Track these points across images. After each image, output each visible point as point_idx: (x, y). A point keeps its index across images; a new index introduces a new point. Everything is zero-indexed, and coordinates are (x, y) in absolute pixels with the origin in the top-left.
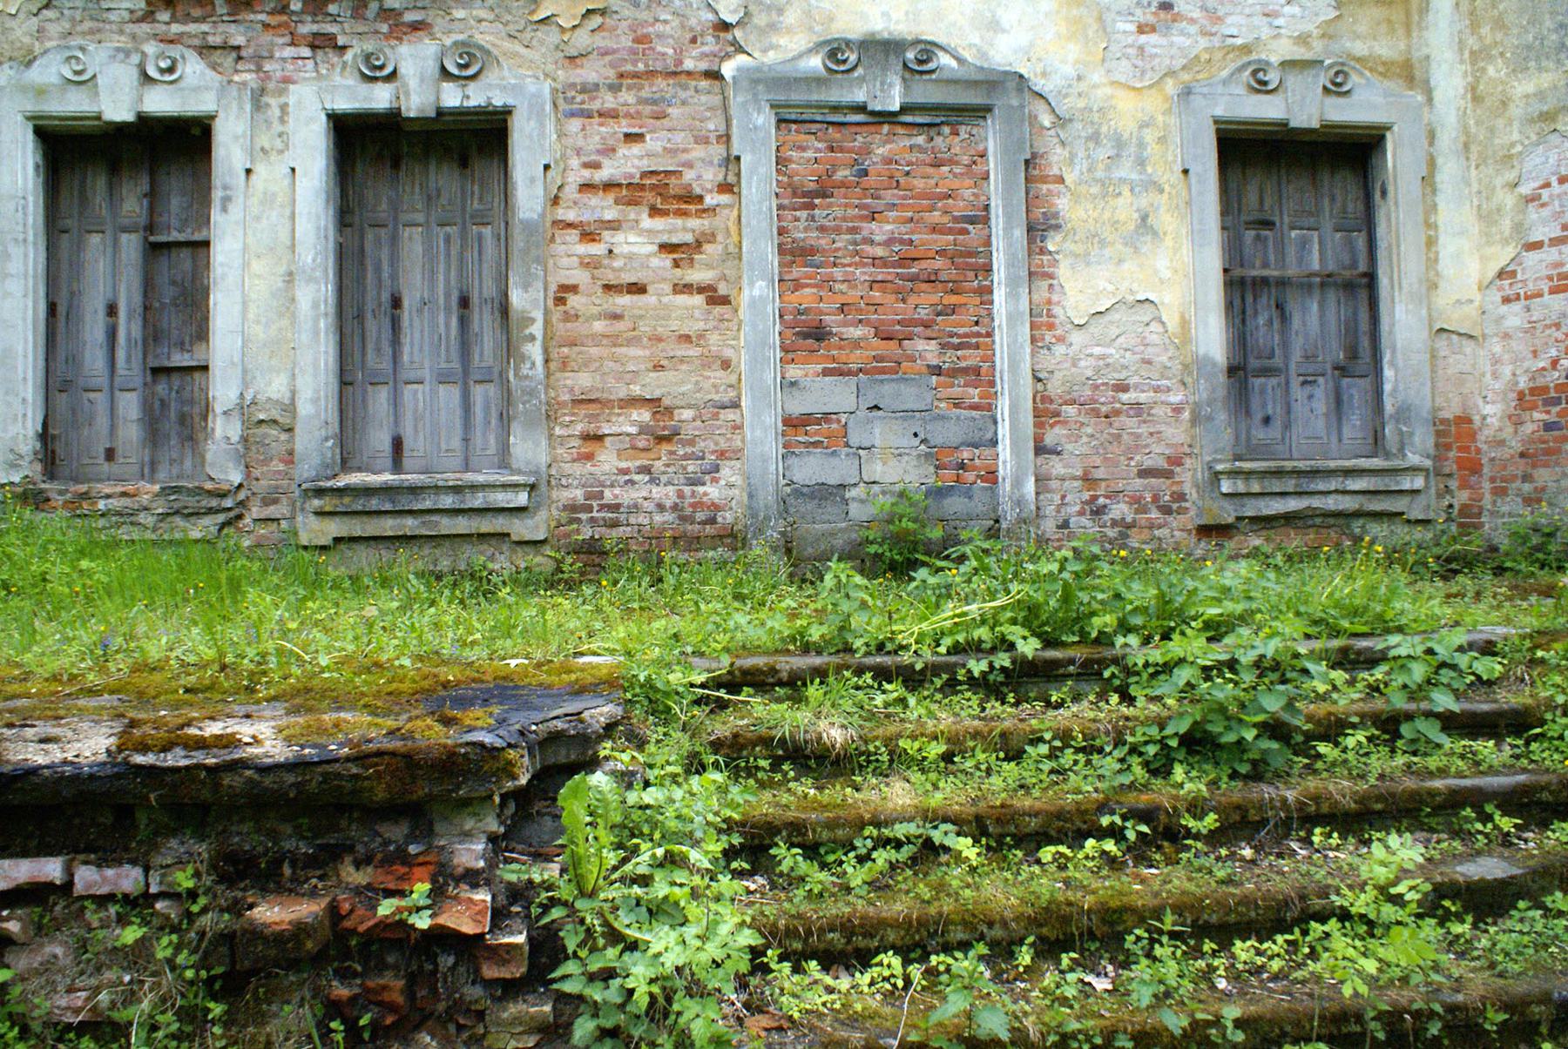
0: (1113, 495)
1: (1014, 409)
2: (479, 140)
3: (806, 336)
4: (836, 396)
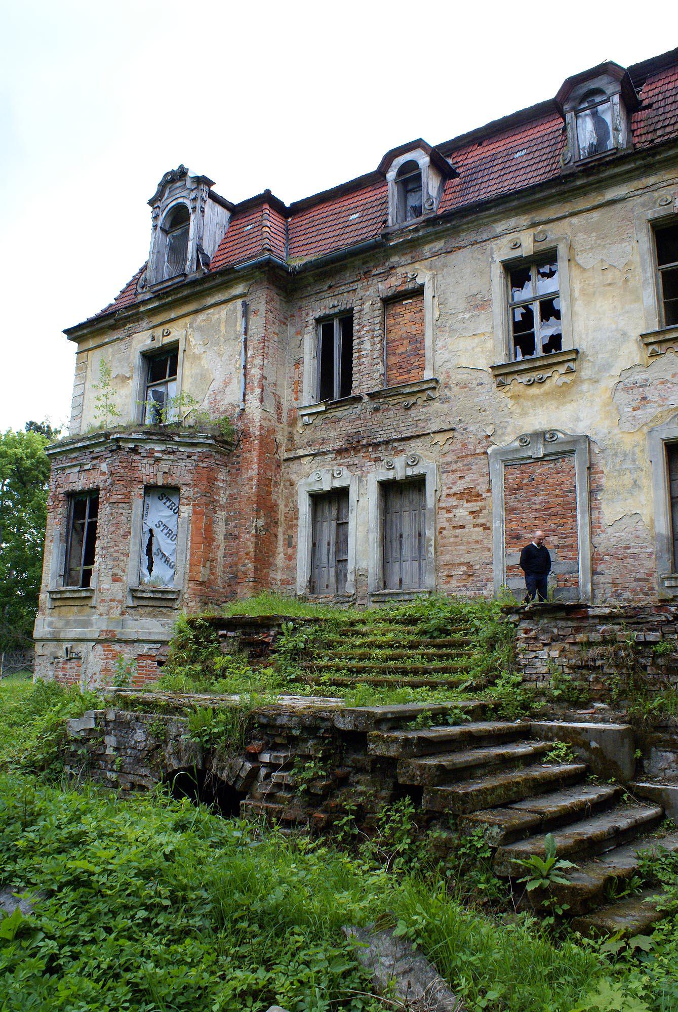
0: (625, 589)
1: (583, 558)
2: (417, 484)
3: (513, 538)
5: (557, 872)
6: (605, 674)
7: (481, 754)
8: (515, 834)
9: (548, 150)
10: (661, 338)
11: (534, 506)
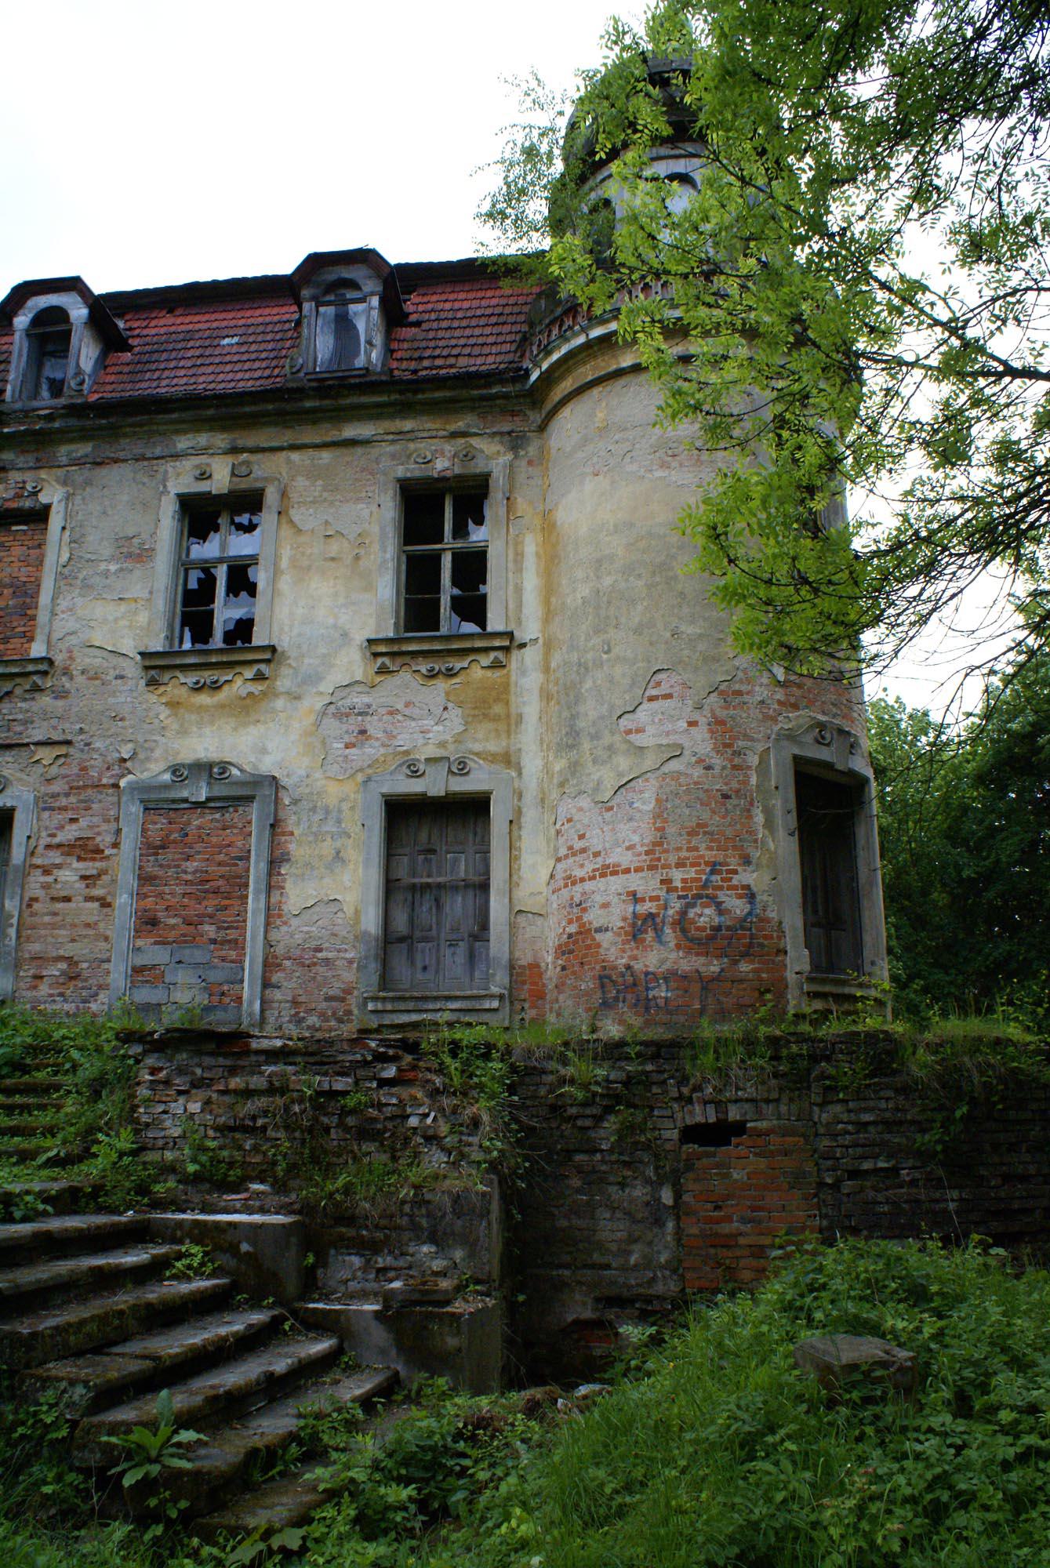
0: (309, 1011)
3: (147, 923)
4: (158, 955)
5: (174, 1450)
6: (268, 1140)
7: (64, 1267)
8: (110, 1395)
9: (270, 346)
10: (395, 649)
11: (185, 876)
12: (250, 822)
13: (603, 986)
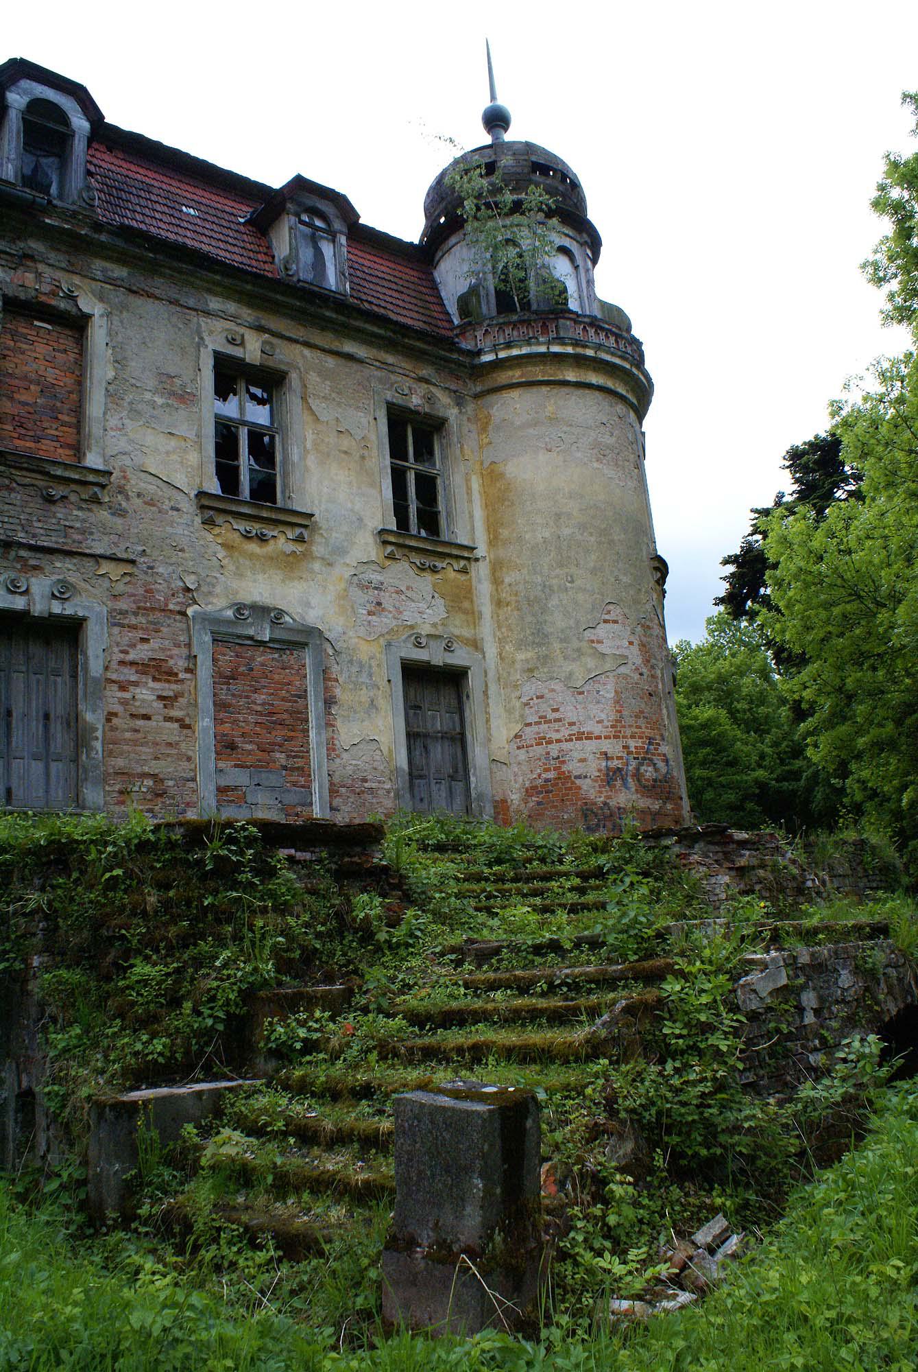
3: (227, 747)
4: (239, 778)
12: (304, 666)
13: (586, 816)
